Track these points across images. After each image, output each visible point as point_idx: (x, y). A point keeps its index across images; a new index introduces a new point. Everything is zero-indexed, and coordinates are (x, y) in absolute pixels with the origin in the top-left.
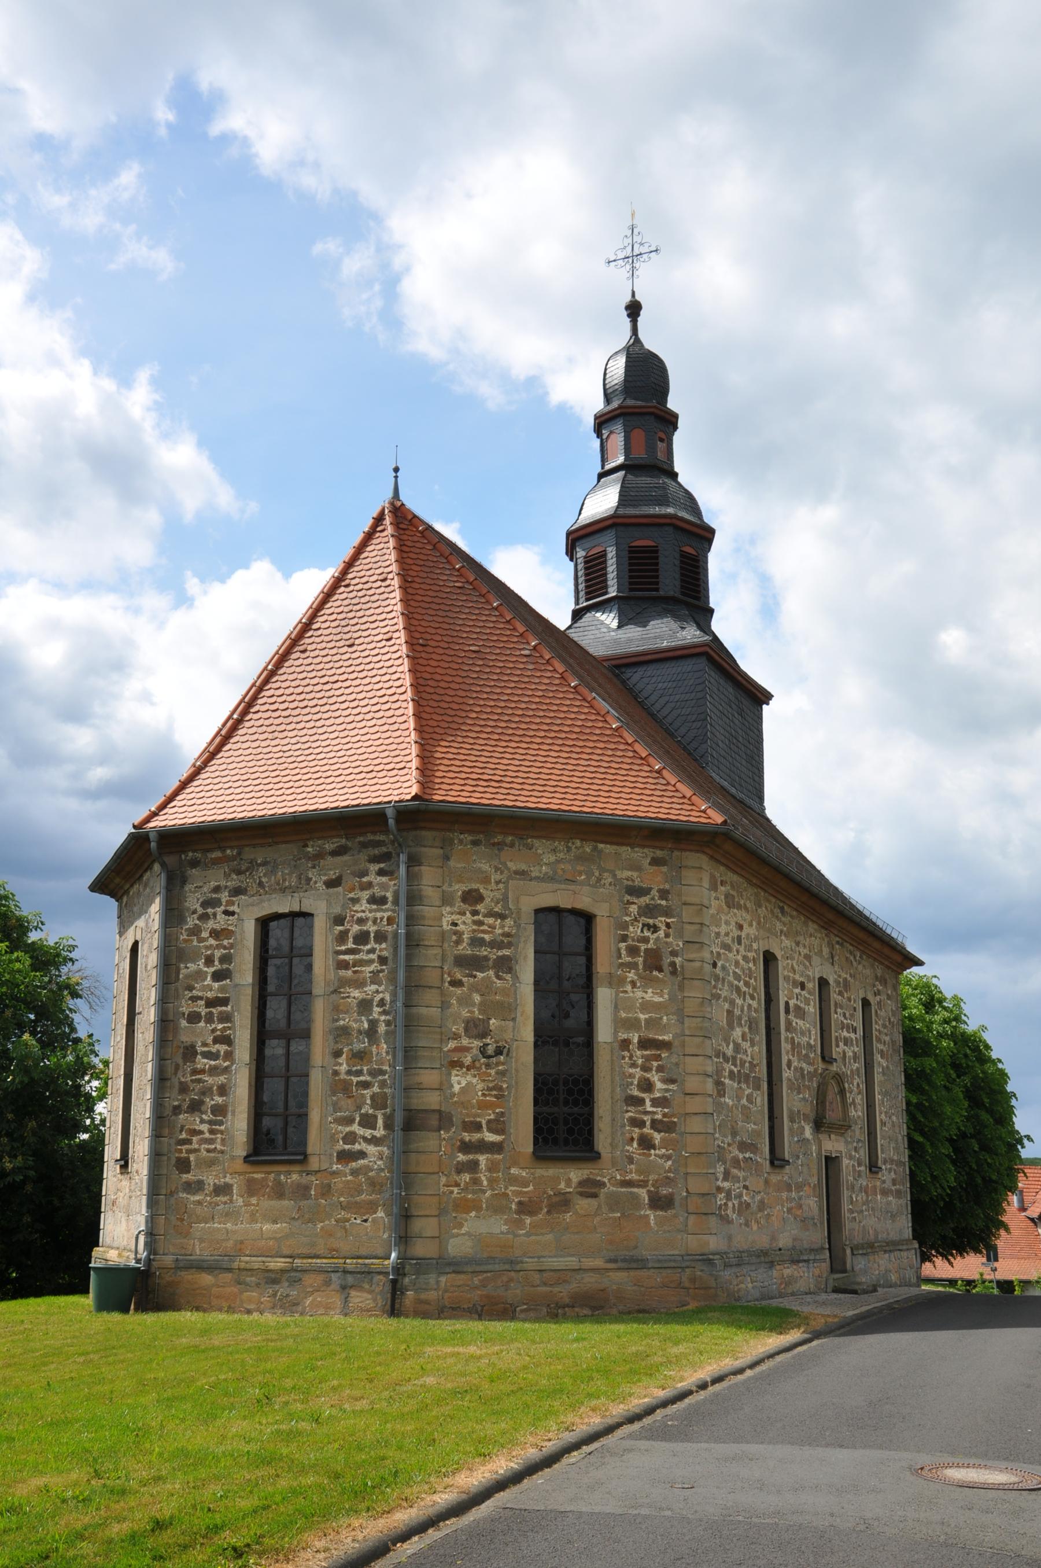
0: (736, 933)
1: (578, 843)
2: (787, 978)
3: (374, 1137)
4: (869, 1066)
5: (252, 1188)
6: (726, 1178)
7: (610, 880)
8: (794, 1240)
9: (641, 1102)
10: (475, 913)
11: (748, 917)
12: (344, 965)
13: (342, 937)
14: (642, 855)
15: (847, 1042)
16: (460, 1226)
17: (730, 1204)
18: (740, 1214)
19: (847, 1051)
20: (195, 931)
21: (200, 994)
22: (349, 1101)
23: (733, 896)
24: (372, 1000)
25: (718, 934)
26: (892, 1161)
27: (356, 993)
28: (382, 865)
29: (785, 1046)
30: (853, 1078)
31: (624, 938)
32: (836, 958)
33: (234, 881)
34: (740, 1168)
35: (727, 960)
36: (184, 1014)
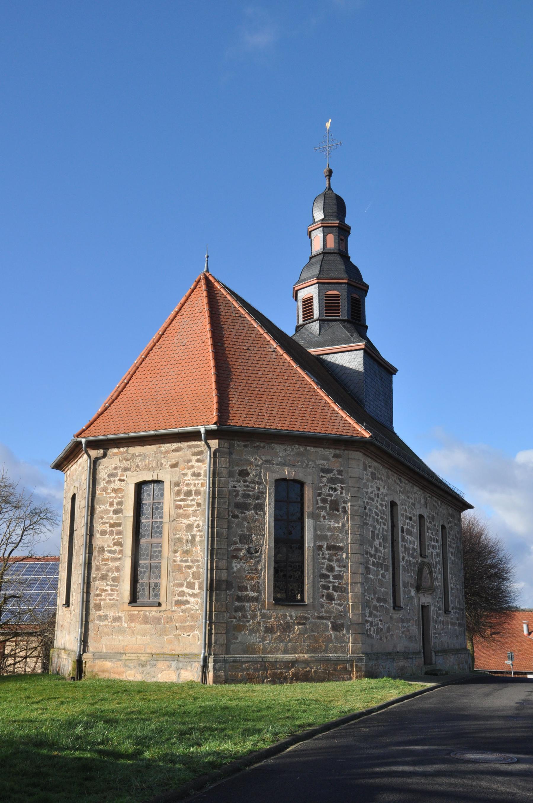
0: (376, 492)
1: (297, 446)
2: (402, 515)
3: (193, 593)
5: (132, 619)
6: (370, 616)
7: (313, 465)
8: (406, 647)
9: (327, 577)
10: (245, 481)
11: (383, 484)
12: (179, 507)
13: (178, 493)
14: (329, 453)
15: (433, 547)
16: (237, 638)
17: (372, 629)
18: (377, 634)
19: (434, 551)
20: (105, 489)
21: (107, 521)
22: (181, 575)
23: (375, 474)
25: (367, 493)
26: (456, 608)
27: (185, 521)
28: (199, 457)
29: (401, 549)
31: (320, 494)
32: (428, 505)
33: (125, 464)
34: (377, 611)
35: (372, 505)
36: (98, 531)
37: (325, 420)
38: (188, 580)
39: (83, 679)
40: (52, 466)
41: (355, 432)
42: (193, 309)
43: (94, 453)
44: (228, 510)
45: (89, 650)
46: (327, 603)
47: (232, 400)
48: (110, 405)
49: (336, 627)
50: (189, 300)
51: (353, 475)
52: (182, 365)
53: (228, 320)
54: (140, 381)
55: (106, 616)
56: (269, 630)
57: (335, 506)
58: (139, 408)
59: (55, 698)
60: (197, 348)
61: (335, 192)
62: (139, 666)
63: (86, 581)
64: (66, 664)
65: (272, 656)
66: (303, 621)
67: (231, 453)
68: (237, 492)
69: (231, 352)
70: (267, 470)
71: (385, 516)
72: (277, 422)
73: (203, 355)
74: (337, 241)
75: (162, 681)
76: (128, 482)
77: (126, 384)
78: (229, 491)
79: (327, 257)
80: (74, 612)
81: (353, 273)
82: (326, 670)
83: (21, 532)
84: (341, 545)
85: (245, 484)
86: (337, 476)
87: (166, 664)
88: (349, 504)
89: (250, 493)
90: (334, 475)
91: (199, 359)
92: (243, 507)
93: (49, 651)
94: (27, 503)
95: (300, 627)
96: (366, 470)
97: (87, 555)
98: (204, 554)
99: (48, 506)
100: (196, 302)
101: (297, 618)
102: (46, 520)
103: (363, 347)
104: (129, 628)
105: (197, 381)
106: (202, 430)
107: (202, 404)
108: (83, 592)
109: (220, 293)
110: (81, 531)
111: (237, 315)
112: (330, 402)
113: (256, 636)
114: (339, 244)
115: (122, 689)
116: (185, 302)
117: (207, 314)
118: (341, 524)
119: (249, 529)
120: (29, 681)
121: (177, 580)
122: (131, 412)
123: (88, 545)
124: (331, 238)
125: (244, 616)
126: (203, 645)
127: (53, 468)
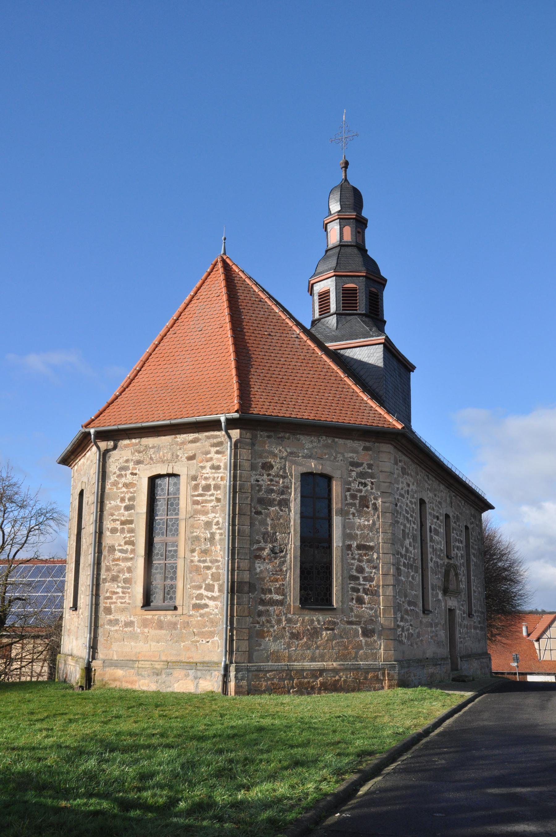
0: (406, 488)
1: (324, 438)
2: (430, 513)
3: (213, 596)
4: (468, 561)
5: (145, 623)
6: (401, 621)
7: (341, 458)
8: (434, 653)
9: (357, 578)
10: (269, 475)
11: (412, 480)
12: (197, 503)
13: (196, 487)
14: (358, 445)
15: (458, 548)
16: (260, 645)
17: (404, 634)
18: (408, 639)
19: (458, 553)
20: (115, 484)
21: (117, 518)
22: (199, 577)
23: (405, 468)
24: (212, 522)
25: (398, 488)
26: (479, 611)
27: (203, 518)
28: (218, 448)
29: (430, 550)
30: (461, 568)
31: (349, 490)
32: (453, 504)
33: (137, 457)
34: (408, 615)
35: (402, 502)
36: (108, 529)
37: (354, 410)
38: (207, 582)
39: (92, 688)
40: (58, 461)
41: (386, 423)
42: (210, 293)
43: (103, 445)
44: (249, 505)
45: (98, 657)
46: (357, 607)
47: (253, 388)
48: (121, 394)
49: (367, 633)
50: (205, 284)
51: (384, 469)
52: (199, 350)
53: (248, 304)
54: (153, 368)
55: (117, 621)
56: (295, 636)
57: (364, 502)
58: (153, 396)
59: (62, 714)
60: (214, 334)
61: (352, 184)
62: (153, 675)
63: (95, 583)
64: (74, 672)
65: (298, 664)
66: (331, 626)
67: (253, 445)
68: (260, 486)
69: (251, 338)
70: (295, 463)
71: (414, 514)
72: (303, 411)
73: (222, 340)
74: (354, 233)
75: (179, 691)
76: (141, 476)
77: (139, 371)
78: (252, 485)
79: (344, 250)
80: (82, 616)
81: (371, 266)
82: (356, 679)
83: (26, 532)
84: (371, 544)
85: (269, 477)
86: (367, 470)
87: (183, 672)
88: (380, 500)
89: (275, 488)
90: (364, 469)
91: (217, 345)
92: (265, 502)
93: (56, 655)
94: (32, 503)
95: (328, 632)
96: (396, 463)
97: (96, 555)
98: (224, 553)
99: (54, 506)
100: (213, 286)
101: (324, 623)
102: (52, 521)
103: (383, 341)
104: (143, 633)
105: (215, 368)
106: (223, 419)
107: (221, 391)
108: (92, 595)
109: (238, 276)
110: (89, 529)
111: (257, 299)
112: (358, 391)
113: (280, 642)
114: (356, 236)
115: (135, 702)
116: (201, 286)
117: (225, 298)
118: (371, 521)
119: (274, 527)
120: (33, 690)
121: (194, 581)
122: (144, 400)
123: (97, 544)
124: (348, 230)
125: (269, 621)
126: (224, 652)
127: (59, 463)
